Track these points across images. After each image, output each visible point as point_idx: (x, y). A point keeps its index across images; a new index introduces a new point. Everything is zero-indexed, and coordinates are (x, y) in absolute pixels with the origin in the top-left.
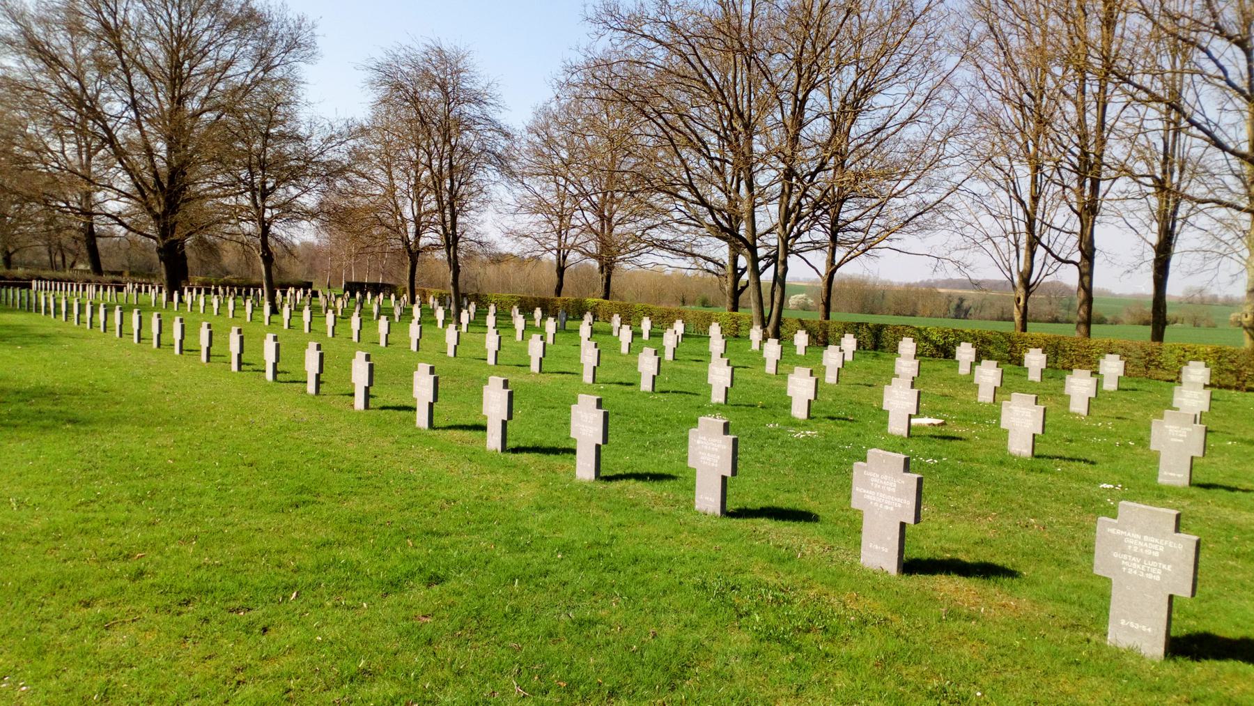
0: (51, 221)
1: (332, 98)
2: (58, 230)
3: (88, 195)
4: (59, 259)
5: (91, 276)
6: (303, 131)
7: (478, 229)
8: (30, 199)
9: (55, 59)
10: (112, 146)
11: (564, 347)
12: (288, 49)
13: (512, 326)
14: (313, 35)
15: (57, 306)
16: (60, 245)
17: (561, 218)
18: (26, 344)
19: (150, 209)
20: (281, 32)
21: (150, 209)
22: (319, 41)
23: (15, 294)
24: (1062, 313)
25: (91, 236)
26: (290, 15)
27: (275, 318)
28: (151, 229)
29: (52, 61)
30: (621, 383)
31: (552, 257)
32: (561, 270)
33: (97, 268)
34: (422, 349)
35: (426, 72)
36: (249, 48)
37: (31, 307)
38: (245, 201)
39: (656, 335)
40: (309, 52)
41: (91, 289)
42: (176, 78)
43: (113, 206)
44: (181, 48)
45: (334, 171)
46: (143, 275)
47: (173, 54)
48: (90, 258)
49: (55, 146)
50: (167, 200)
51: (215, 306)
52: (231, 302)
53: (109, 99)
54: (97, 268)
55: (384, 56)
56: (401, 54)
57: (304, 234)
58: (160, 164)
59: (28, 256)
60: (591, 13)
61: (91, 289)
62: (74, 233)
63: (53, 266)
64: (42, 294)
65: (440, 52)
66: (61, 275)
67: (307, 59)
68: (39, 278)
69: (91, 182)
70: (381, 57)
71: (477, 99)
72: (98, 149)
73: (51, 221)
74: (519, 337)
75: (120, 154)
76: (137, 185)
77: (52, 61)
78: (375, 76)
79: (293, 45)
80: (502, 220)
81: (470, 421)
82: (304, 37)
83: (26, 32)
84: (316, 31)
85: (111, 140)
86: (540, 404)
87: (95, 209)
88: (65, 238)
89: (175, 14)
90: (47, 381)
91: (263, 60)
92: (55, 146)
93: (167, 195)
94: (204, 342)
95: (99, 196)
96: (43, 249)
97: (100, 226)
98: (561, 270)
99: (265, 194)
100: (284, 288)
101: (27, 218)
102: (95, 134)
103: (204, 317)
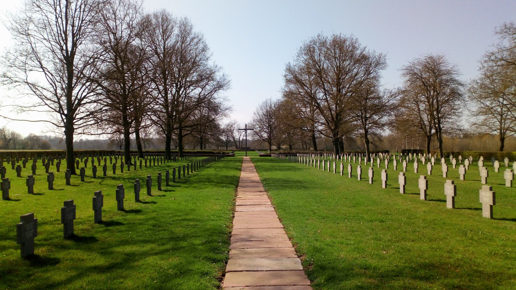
0: (303, 134)
1: (391, 82)
2: (304, 137)
3: (313, 125)
4: (305, 146)
5: (314, 152)
6: (381, 94)
7: (458, 124)
8: (297, 128)
9: (303, 84)
10: (319, 109)
11: (437, 166)
12: (376, 66)
13: (451, 164)
14: (385, 59)
15: (303, 161)
16: (305, 142)
17: (501, 116)
18: (295, 171)
19: (330, 128)
20: (373, 60)
21: (330, 128)
22: (387, 61)
23: (293, 158)
24: (115, 149)
25: (314, 138)
26: (376, 54)
27: (368, 163)
28: (331, 135)
29: (302, 84)
30: (500, 184)
31: (497, 133)
32: (502, 139)
33: (316, 149)
34: (421, 173)
35: (425, 66)
36: (363, 68)
37: (296, 161)
38: (359, 122)
39: (463, 161)
40: (384, 65)
41: (313, 156)
42: (338, 84)
43: (320, 128)
44: (340, 71)
45: (394, 107)
46: (329, 151)
47: (338, 75)
48: (313, 146)
49: (304, 109)
50: (335, 124)
51: (354, 160)
52: (360, 158)
53: (319, 92)
54: (316, 149)
55: (409, 64)
56: (416, 62)
57: (386, 132)
58: (333, 112)
59: (296, 146)
60: (498, 29)
61: (313, 156)
62: (309, 138)
63: (303, 149)
64: (299, 158)
65: (431, 58)
66: (305, 152)
67: (382, 68)
68: (299, 153)
69: (313, 121)
70: (407, 64)
71: (448, 73)
72: (316, 109)
73: (303, 134)
74: (454, 167)
75: (322, 112)
76: (326, 120)
77: (302, 84)
78: (405, 72)
79: (378, 64)
80: (466, 118)
81: (396, 187)
82: (382, 61)
83: (295, 77)
84: (386, 58)
85: (318, 107)
86: (466, 194)
87: (315, 129)
88: (306, 139)
89: (338, 62)
90: (299, 179)
91: (368, 72)
92: (304, 109)
93: (336, 122)
94: (341, 169)
95: (316, 125)
96: (301, 144)
97: (317, 135)
98: (502, 139)
99: (366, 119)
100: (377, 153)
101: (296, 134)
102: (315, 105)
103: (349, 166)
